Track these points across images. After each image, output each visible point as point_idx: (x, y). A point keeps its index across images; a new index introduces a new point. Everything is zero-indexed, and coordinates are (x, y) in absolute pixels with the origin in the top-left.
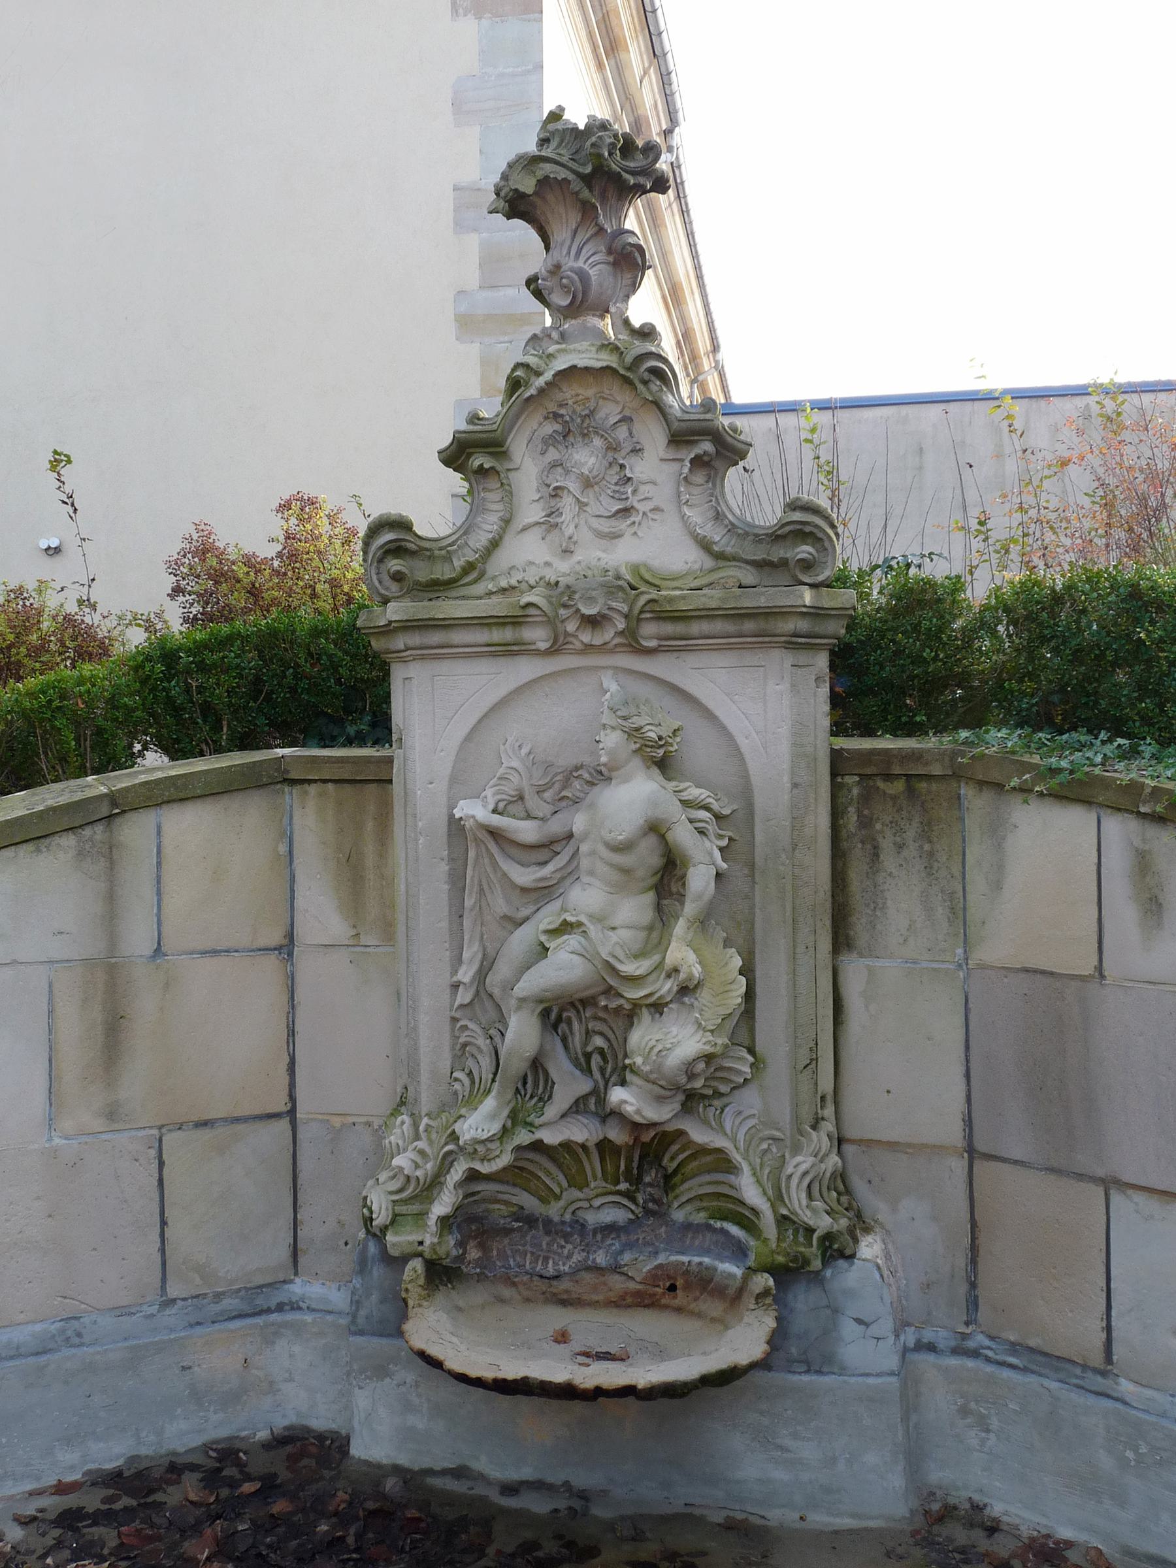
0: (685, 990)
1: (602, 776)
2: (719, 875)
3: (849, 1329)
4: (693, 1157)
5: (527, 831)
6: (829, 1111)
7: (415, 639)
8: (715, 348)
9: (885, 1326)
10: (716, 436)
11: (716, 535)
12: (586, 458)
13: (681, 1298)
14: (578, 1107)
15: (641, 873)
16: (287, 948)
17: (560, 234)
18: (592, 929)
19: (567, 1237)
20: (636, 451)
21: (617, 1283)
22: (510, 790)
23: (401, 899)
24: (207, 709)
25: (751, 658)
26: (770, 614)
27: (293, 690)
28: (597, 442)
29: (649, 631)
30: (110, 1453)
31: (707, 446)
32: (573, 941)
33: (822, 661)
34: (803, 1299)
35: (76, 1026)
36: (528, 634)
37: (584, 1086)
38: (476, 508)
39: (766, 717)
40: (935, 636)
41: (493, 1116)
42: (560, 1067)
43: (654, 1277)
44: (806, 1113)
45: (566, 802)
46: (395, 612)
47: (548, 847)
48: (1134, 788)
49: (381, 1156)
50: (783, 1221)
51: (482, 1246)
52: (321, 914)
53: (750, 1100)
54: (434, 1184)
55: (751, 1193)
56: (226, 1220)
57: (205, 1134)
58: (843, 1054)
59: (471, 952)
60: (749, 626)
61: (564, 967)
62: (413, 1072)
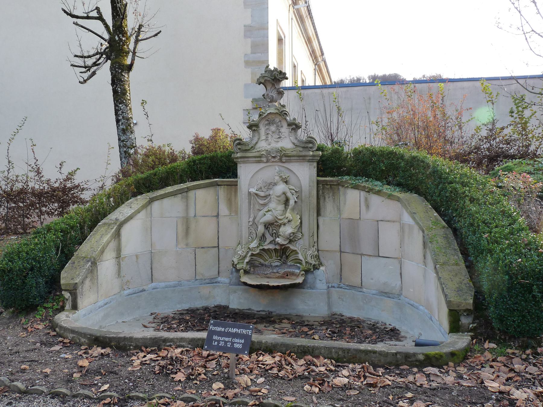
0: (289, 221)
1: (275, 184)
2: (295, 202)
3: (318, 281)
4: (291, 252)
5: (262, 194)
6: (316, 244)
7: (242, 160)
8: (322, 54)
9: (324, 281)
10: (296, 125)
11: (296, 142)
12: (273, 128)
13: (289, 277)
14: (271, 242)
15: (282, 201)
16: (217, 216)
17: (269, 88)
18: (273, 211)
19: (269, 268)
20: (282, 127)
21: (278, 275)
22: (259, 187)
23: (239, 207)
24: (201, 171)
25: (302, 164)
26: (305, 156)
27: (217, 167)
28: (275, 125)
29: (284, 159)
30: (186, 306)
31: (294, 126)
32: (270, 213)
33: (315, 164)
34: (310, 276)
35: (181, 229)
36: (262, 159)
37: (272, 239)
38: (253, 136)
39: (305, 174)
40: (339, 159)
41: (256, 244)
42: (268, 235)
43: (284, 273)
44: (312, 245)
45: (269, 189)
46: (239, 155)
47: (266, 197)
48: (364, 187)
49: (235, 253)
50: (307, 262)
51: (253, 268)
52: (224, 209)
53: (301, 242)
54: (245, 257)
55: (301, 257)
56: (207, 266)
57: (203, 249)
58: (319, 235)
59: (252, 216)
60: (301, 158)
61: (268, 217)
62: (241, 237)
